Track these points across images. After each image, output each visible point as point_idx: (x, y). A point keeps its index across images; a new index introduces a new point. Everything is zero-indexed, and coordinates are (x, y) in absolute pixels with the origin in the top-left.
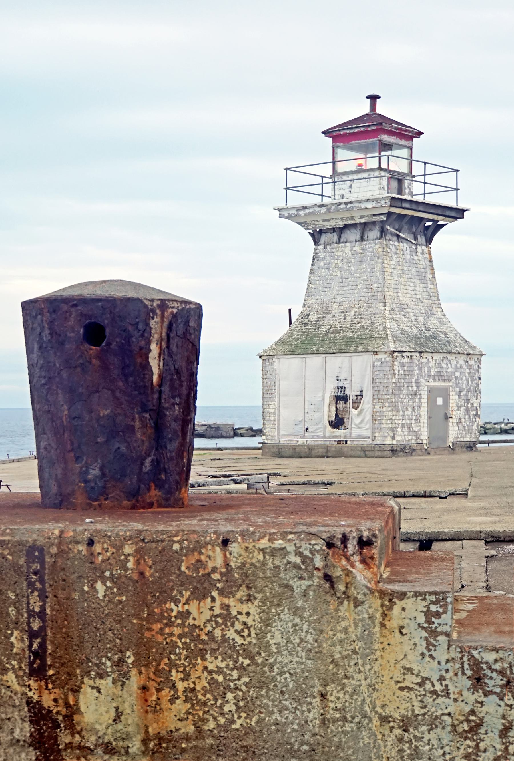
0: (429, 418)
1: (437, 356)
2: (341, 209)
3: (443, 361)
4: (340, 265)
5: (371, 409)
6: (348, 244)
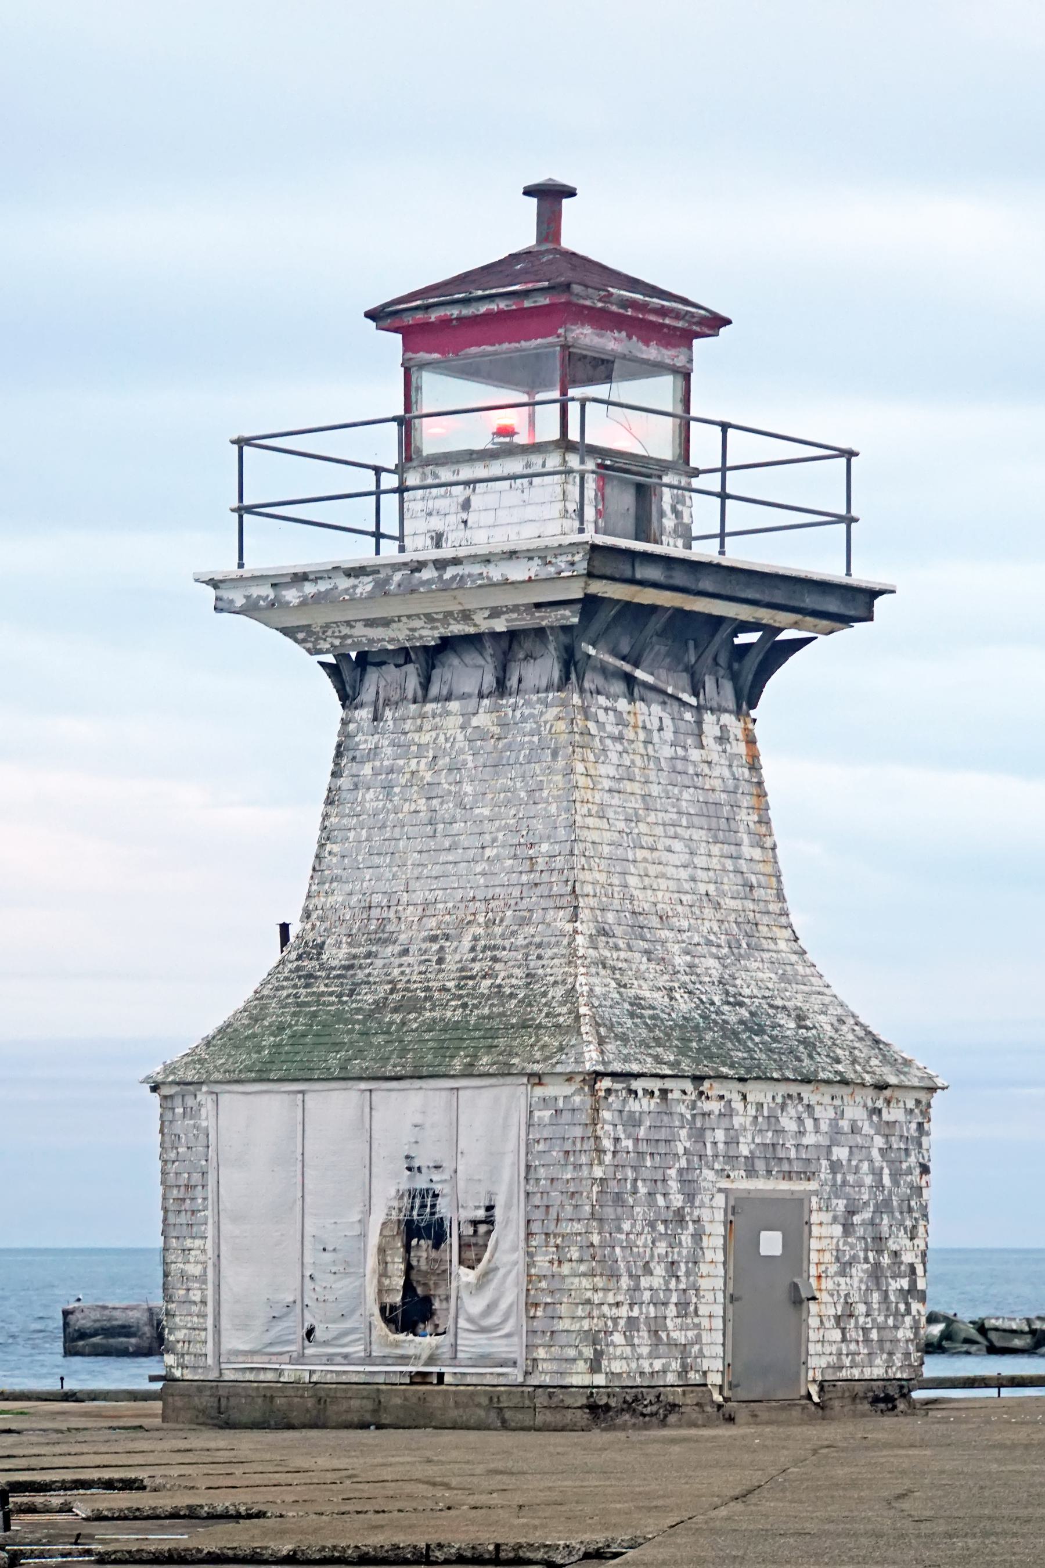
0: (733, 1299)
1: (758, 1093)
2: (423, 583)
3: (783, 1107)
4: (428, 777)
5: (521, 1267)
6: (454, 706)
